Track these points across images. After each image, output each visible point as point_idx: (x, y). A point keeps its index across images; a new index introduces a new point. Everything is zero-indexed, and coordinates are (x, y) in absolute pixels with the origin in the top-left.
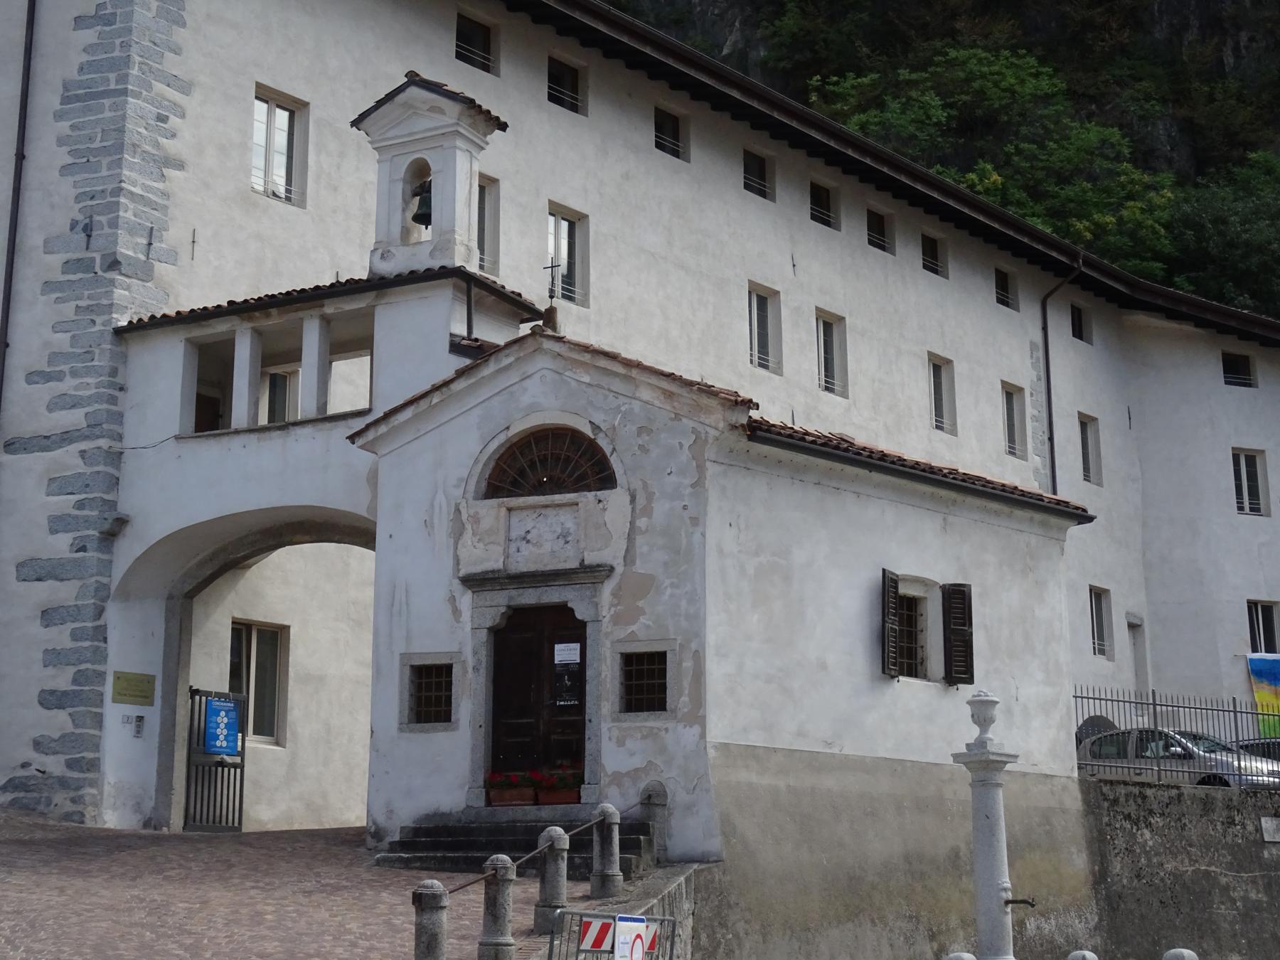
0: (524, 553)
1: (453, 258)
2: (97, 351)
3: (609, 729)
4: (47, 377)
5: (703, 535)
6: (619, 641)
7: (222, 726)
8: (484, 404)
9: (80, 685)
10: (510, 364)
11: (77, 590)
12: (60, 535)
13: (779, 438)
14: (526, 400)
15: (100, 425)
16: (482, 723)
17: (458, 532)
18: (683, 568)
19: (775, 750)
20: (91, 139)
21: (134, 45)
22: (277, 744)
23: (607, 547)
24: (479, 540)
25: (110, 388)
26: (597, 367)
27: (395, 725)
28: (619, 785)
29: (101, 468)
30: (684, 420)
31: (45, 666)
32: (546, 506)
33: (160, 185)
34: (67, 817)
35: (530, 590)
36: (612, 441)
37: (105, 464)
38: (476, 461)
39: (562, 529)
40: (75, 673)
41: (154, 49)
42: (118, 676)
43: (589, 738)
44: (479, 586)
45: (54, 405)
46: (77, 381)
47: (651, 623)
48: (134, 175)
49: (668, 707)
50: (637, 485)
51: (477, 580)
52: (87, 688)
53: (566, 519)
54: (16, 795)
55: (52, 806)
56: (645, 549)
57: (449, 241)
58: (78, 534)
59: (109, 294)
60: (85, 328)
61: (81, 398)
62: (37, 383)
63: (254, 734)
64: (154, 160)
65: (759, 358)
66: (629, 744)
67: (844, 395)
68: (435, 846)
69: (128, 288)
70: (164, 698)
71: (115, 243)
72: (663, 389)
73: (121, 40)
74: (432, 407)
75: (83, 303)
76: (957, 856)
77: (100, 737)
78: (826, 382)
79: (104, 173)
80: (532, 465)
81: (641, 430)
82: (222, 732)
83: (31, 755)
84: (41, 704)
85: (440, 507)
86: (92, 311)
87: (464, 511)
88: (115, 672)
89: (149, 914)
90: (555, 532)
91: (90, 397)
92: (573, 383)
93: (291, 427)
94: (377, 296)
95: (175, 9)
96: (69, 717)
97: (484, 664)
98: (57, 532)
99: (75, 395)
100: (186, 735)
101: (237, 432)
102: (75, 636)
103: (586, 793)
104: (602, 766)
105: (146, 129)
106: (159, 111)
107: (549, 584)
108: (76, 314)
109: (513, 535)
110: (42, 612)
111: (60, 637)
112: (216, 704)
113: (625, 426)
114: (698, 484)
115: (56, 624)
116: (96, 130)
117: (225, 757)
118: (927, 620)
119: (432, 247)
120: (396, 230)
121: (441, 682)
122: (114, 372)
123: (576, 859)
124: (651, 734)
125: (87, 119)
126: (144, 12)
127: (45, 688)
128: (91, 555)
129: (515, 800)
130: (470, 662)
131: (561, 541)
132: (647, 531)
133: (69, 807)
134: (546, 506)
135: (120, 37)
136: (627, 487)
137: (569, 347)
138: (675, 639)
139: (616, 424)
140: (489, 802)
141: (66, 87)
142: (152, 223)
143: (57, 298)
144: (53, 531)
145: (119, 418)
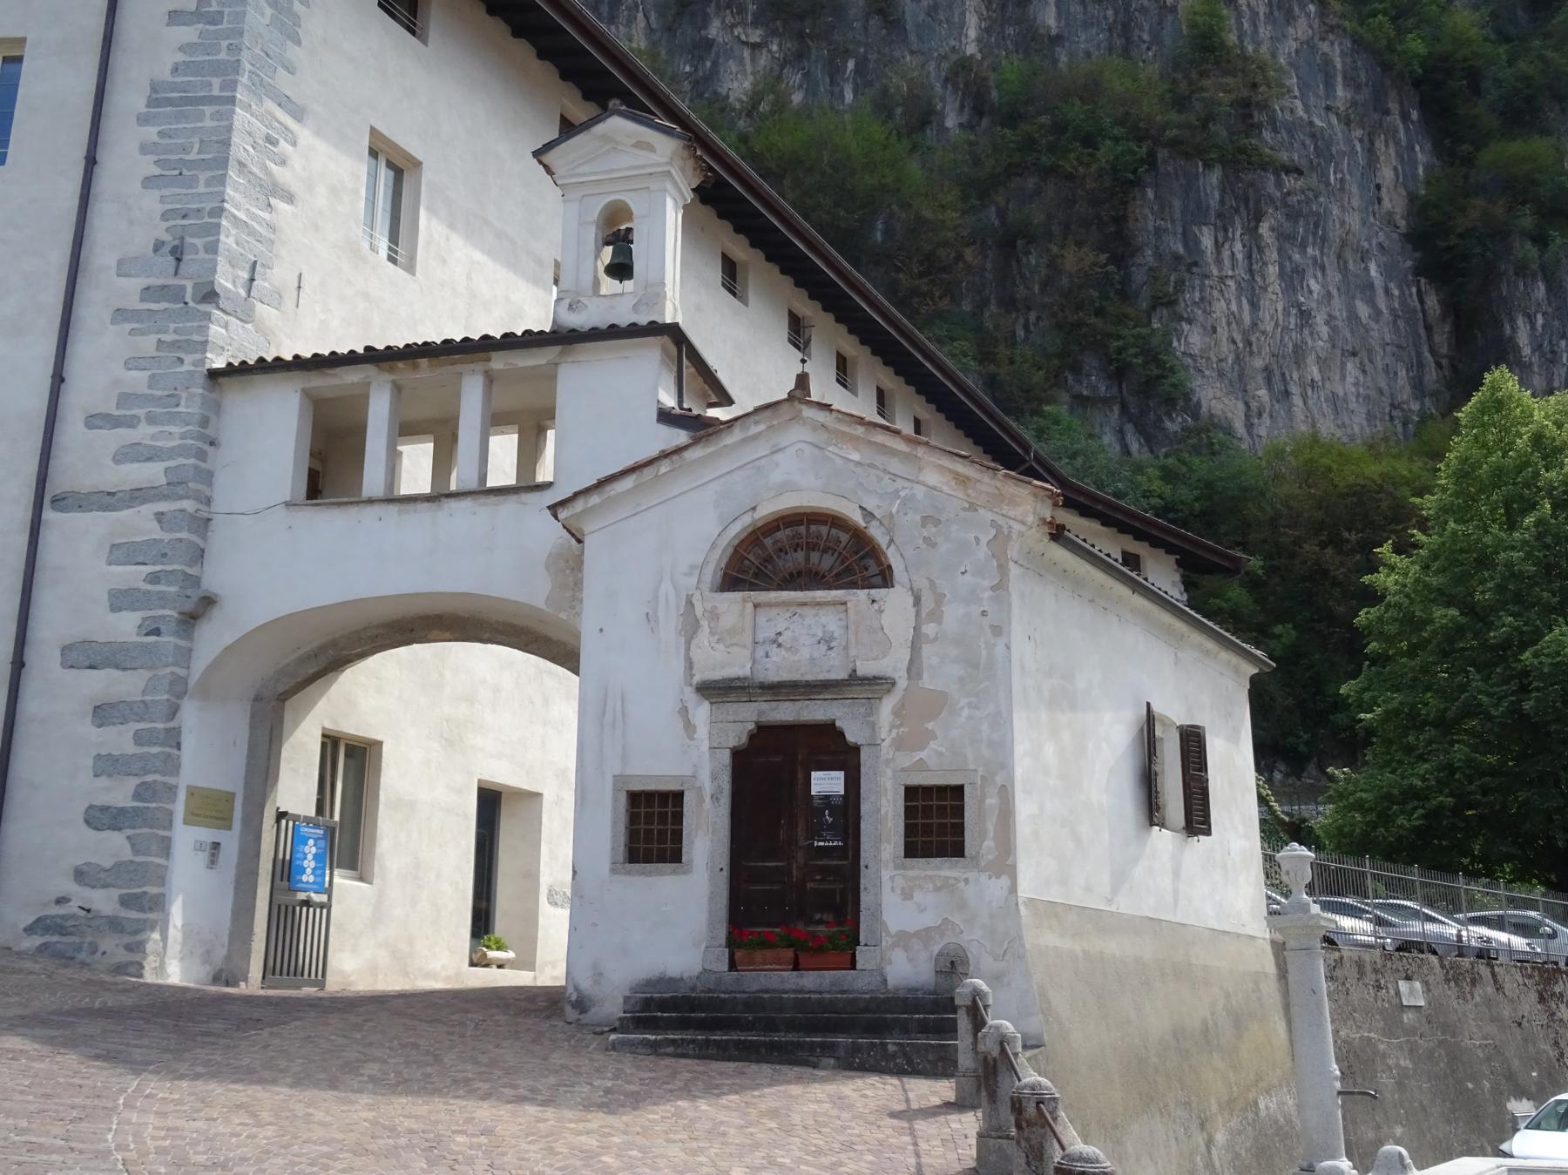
1: (664, 315)
2: (184, 395)
3: (892, 878)
4: (115, 422)
5: (1008, 647)
6: (903, 770)
7: (310, 857)
8: (722, 480)
10: (760, 433)
12: (124, 614)
14: (776, 477)
17: (690, 628)
18: (982, 686)
19: (1070, 907)
21: (245, 50)
22: (361, 879)
23: (884, 656)
24: (718, 641)
26: (870, 442)
27: (607, 866)
28: (906, 949)
29: (184, 535)
30: (981, 511)
31: (96, 776)
32: (804, 604)
33: (266, 215)
34: (120, 969)
35: (787, 703)
36: (889, 531)
37: (190, 531)
38: (714, 546)
39: (824, 632)
40: (138, 786)
42: (192, 792)
43: (866, 889)
45: (121, 457)
46: (153, 430)
47: (944, 750)
48: (238, 197)
49: (966, 853)
50: (922, 584)
51: (719, 688)
52: (154, 805)
53: (830, 621)
55: (99, 954)
56: (935, 661)
57: (658, 295)
59: (204, 330)
61: (161, 449)
62: (101, 428)
64: (261, 186)
66: (917, 896)
68: (683, 1024)
69: (226, 326)
70: (246, 821)
71: (214, 271)
72: (957, 474)
76: (1207, 1029)
77: (167, 867)
79: (201, 189)
81: (926, 520)
82: (309, 864)
83: (69, 887)
84: (87, 822)
85: (667, 600)
86: (179, 347)
88: (189, 787)
90: (813, 635)
91: (172, 449)
92: (839, 461)
93: (443, 499)
98: (120, 609)
99: (151, 446)
100: (270, 866)
101: (371, 501)
102: (139, 739)
103: (863, 956)
104: (883, 923)
105: (254, 148)
108: (157, 350)
111: (120, 740)
112: (305, 830)
113: (906, 514)
114: (1000, 587)
115: (114, 724)
117: (313, 895)
118: (1163, 764)
120: (587, 280)
122: (204, 422)
123: (890, 1047)
124: (944, 886)
125: (180, 126)
127: (94, 803)
128: (167, 639)
129: (769, 963)
131: (823, 647)
132: (936, 639)
133: (122, 956)
134: (804, 604)
135: (227, 38)
136: (909, 586)
137: (837, 418)
138: (976, 770)
140: (733, 965)
141: (154, 87)
142: (255, 256)
144: (115, 608)
145: (208, 477)
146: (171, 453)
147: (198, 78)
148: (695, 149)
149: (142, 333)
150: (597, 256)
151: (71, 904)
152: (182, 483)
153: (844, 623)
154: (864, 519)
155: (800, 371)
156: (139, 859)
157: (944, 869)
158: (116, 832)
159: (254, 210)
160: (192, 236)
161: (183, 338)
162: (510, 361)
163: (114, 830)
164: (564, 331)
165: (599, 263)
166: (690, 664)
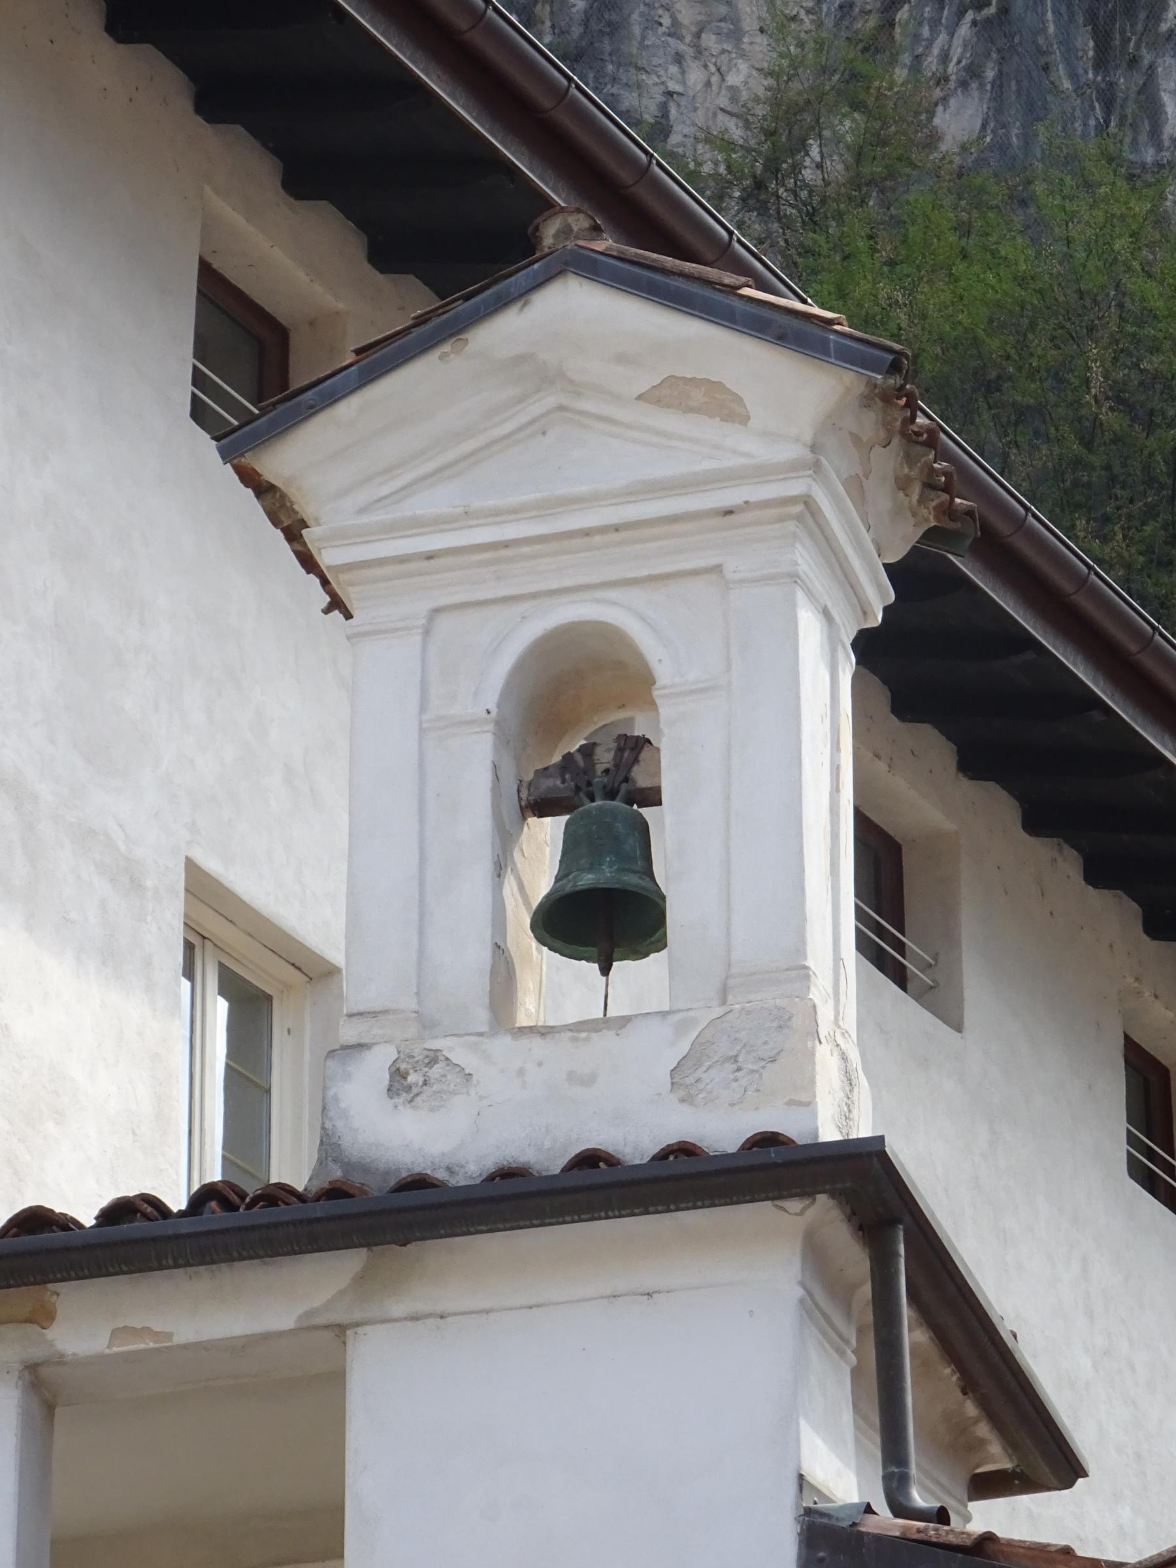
57: (782, 1021)
94: (360, 1279)
119: (684, 1047)
148: (912, 406)
150: (501, 866)
162: (136, 1322)
164: (376, 1187)
165: (510, 888)
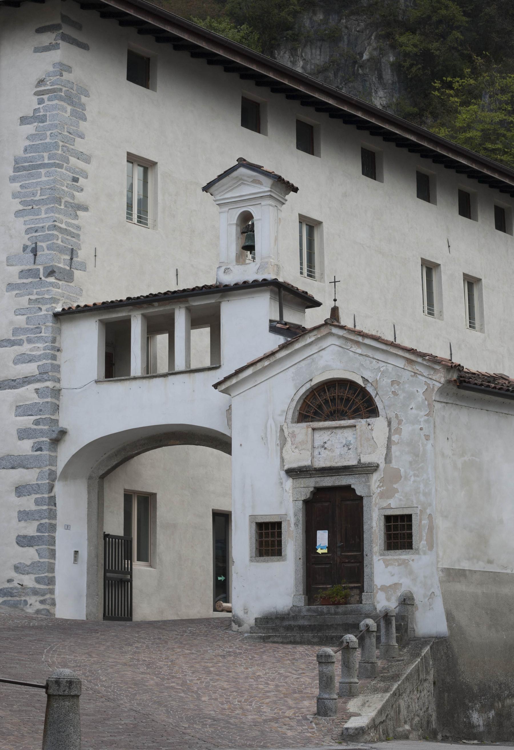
0: (323, 455)
2: (43, 327)
4: (12, 343)
6: (383, 509)
8: (296, 366)
9: (42, 532)
11: (37, 475)
13: (475, 386)
14: (322, 363)
15: (47, 373)
16: (301, 557)
17: (283, 441)
18: (421, 465)
19: (475, 572)
20: (34, 195)
22: (151, 566)
25: (52, 350)
29: (49, 400)
31: (19, 521)
32: (336, 428)
35: (328, 478)
36: (376, 389)
38: (292, 400)
39: (346, 441)
41: (70, 137)
43: (366, 566)
44: (297, 475)
45: (17, 361)
49: (413, 548)
53: (348, 435)
54: (5, 599)
55: (28, 605)
56: (398, 453)
58: (36, 440)
60: (35, 313)
61: (35, 356)
62: (6, 347)
63: (138, 560)
64: (72, 206)
65: (428, 309)
67: (482, 330)
73: (50, 132)
74: (265, 368)
75: (33, 297)
78: (470, 323)
79: (43, 216)
80: (326, 402)
83: (13, 574)
84: (17, 543)
86: (39, 302)
87: (286, 431)
89: (148, 668)
91: (40, 356)
95: (81, 110)
96: (35, 552)
97: (301, 522)
99: (30, 355)
101: (135, 378)
102: (37, 502)
106: (74, 175)
107: (340, 474)
109: (316, 444)
110: (16, 488)
115: (25, 496)
116: (37, 189)
121: (274, 532)
122: (54, 340)
124: (404, 563)
125: (30, 181)
126: (63, 114)
127: (20, 534)
130: (292, 520)
131: (346, 449)
134: (336, 428)
135: (50, 130)
139: (378, 378)
141: (16, 161)
142: (72, 246)
143: (17, 294)
144: (20, 438)
145: (57, 368)
146: (39, 358)
147: (37, 154)
149: (21, 295)
151: (14, 582)
152: (46, 373)
153: (355, 436)
154: (364, 383)
155: (333, 306)
156: (42, 560)
157: (403, 555)
158: (31, 548)
159: (70, 221)
160: (41, 241)
161: (41, 297)
163: (29, 547)
166: (282, 460)
